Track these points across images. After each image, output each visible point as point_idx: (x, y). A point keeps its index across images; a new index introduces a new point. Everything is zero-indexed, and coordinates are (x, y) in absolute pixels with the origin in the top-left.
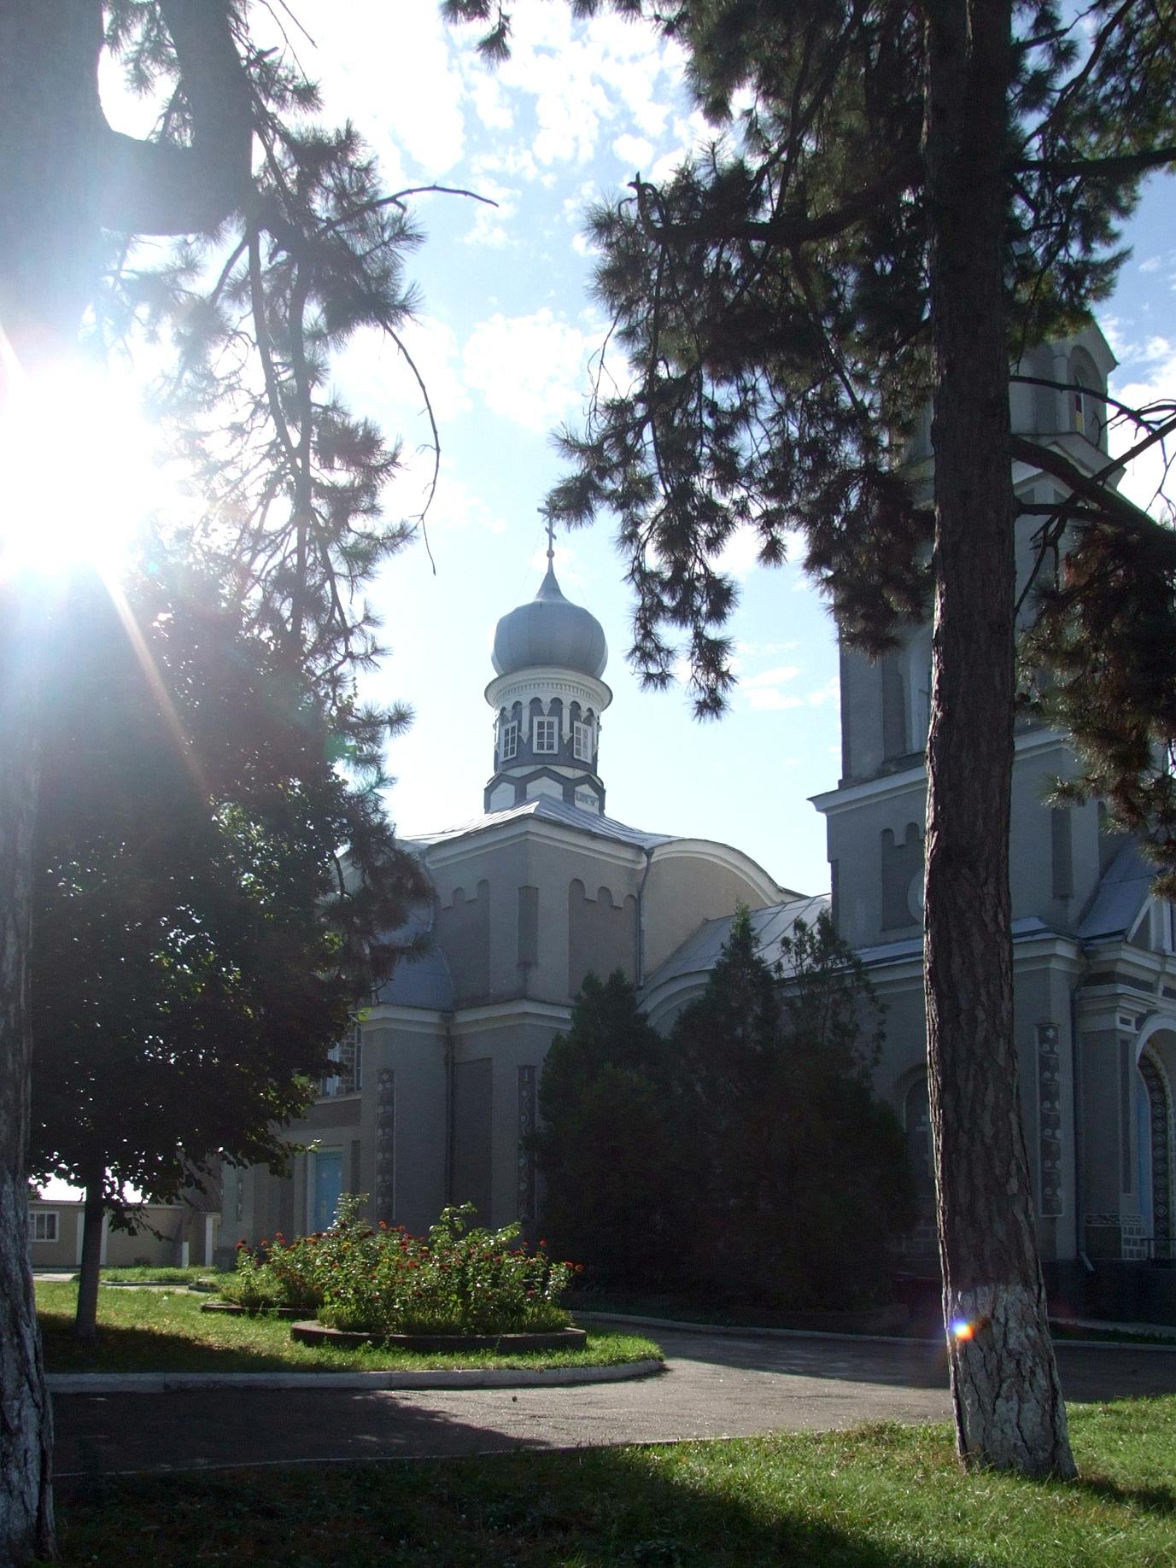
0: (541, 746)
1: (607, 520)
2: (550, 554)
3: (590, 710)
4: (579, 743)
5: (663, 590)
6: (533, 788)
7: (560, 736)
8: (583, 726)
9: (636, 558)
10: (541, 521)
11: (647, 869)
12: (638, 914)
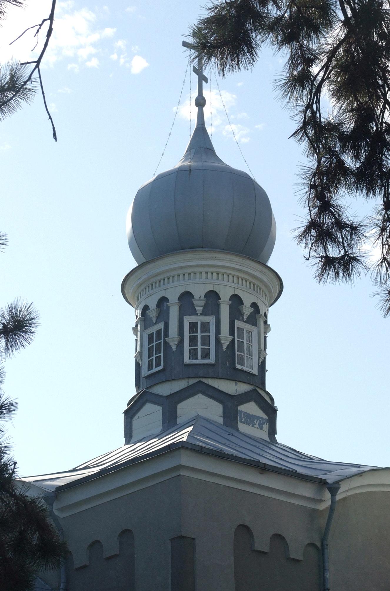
0: (193, 354)
1: (272, 58)
2: (200, 102)
3: (254, 305)
4: (241, 350)
5: (344, 148)
6: (186, 409)
7: (218, 341)
8: (246, 327)
9: (309, 106)
10: (186, 58)
11: (332, 509)
12: (322, 568)
